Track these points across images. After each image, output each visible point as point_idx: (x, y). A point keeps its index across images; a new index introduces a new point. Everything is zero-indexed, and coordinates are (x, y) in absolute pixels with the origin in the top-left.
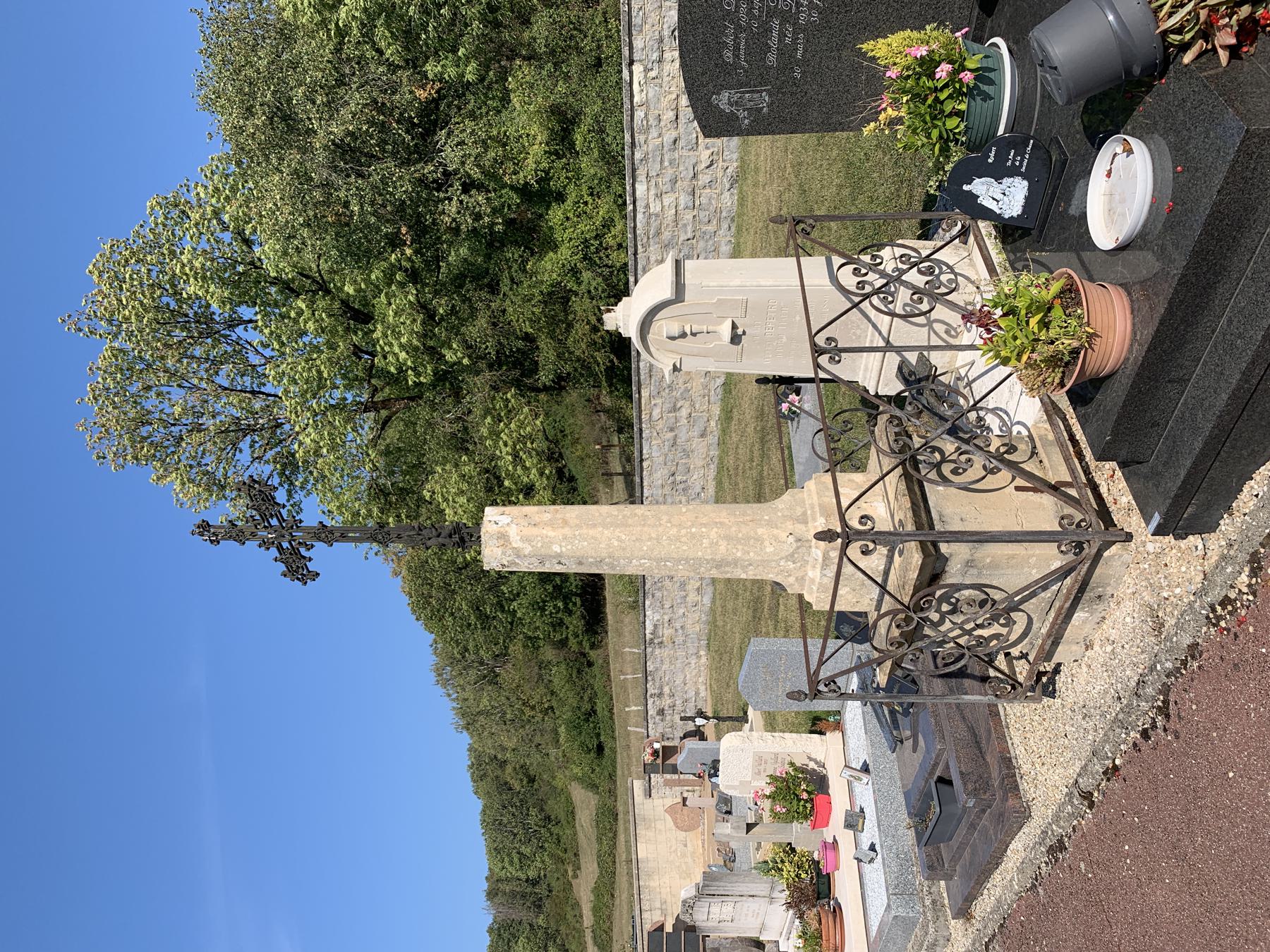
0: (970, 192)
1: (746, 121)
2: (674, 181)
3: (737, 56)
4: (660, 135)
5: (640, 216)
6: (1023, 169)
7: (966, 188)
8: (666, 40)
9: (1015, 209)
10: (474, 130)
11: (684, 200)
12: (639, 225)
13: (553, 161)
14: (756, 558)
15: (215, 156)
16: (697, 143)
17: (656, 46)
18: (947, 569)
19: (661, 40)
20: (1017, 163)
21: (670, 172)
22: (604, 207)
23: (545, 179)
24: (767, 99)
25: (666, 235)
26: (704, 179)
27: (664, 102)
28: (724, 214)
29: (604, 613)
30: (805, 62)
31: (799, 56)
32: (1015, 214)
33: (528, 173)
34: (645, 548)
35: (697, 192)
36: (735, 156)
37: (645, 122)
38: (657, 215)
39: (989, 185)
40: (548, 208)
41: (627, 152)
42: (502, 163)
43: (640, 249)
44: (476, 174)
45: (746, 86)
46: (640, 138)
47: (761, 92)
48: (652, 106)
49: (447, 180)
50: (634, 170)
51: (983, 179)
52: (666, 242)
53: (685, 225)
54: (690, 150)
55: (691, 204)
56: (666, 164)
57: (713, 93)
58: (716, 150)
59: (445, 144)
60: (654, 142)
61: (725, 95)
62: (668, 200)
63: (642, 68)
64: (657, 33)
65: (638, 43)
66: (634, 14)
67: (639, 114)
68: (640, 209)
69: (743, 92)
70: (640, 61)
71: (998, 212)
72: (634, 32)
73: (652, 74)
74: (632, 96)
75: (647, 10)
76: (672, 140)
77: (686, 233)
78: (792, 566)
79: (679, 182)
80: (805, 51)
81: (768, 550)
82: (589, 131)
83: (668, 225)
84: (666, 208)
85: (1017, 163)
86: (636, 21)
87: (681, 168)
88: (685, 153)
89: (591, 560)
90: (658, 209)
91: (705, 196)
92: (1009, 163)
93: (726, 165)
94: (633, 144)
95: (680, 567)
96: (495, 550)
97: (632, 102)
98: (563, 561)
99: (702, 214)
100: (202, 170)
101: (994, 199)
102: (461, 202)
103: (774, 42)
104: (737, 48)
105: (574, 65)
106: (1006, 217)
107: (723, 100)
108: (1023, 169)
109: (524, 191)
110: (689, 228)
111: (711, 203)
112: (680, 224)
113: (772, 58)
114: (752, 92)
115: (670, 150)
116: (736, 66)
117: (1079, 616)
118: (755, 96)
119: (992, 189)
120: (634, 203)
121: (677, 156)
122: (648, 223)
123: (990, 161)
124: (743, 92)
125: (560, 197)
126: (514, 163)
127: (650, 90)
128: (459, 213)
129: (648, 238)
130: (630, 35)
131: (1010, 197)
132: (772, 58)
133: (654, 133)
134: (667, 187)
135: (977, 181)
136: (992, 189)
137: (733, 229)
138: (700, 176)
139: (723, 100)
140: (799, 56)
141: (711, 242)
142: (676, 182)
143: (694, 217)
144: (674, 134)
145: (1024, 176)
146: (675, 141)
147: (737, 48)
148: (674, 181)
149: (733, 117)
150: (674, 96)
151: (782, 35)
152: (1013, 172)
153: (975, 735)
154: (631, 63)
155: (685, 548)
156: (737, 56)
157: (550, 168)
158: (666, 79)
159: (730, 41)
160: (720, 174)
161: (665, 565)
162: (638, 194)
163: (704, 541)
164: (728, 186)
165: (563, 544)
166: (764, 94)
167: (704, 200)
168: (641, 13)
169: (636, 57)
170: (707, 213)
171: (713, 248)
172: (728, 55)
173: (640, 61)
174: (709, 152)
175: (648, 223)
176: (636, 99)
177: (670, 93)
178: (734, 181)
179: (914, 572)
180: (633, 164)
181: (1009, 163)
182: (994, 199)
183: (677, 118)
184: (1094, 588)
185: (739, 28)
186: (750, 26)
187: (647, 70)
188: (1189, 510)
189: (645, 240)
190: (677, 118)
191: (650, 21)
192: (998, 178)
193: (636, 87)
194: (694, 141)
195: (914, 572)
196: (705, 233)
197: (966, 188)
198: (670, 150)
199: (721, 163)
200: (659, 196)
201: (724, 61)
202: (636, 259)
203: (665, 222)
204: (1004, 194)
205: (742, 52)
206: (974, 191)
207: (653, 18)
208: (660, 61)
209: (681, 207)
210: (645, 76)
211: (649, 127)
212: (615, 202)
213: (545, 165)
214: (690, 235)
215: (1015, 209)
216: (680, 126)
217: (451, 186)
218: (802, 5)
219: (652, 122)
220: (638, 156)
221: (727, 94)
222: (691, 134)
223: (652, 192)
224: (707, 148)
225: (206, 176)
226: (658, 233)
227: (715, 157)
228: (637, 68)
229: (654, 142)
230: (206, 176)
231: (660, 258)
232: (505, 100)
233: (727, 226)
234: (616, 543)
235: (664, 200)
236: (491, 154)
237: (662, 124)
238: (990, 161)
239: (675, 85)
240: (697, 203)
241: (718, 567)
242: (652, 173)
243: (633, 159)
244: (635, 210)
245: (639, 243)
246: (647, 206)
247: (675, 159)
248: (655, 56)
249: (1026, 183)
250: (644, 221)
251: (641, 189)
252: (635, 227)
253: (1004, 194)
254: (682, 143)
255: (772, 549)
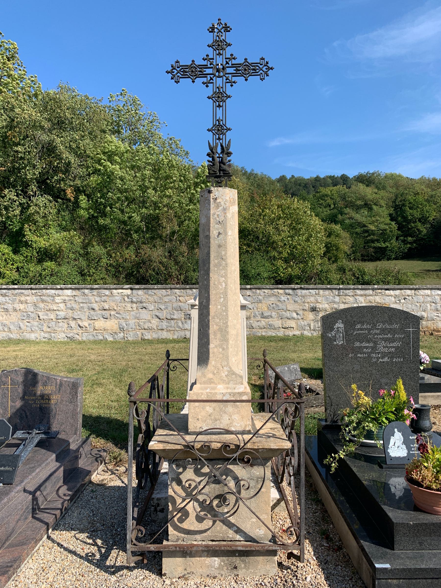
0: (394, 432)
1: (330, 335)
2: (72, 309)
3: (358, 330)
4: (96, 302)
5: (53, 291)
6: (411, 452)
7: (396, 430)
8: (141, 305)
9: (393, 454)
10: (51, 213)
11: (62, 314)
12: (48, 291)
13: (36, 250)
14: (230, 352)
15: (41, 86)
16: (92, 320)
17: (139, 300)
18: (255, 467)
19: (141, 302)
20: (413, 449)
21: (76, 306)
22: (15, 275)
23: (27, 245)
24: (340, 343)
25: (42, 305)
26: (73, 324)
27: (113, 304)
28: (53, 335)
29: (419, 260)
30: (356, 358)
31: (359, 355)
32: (391, 454)
33: (30, 236)
34: (231, 286)
35: (66, 321)
36: (84, 338)
37: (103, 295)
38: (53, 300)
39: (400, 440)
40: (8, 245)
41: (89, 286)
42: (35, 224)
43: (34, 291)
44: (32, 210)
45: (346, 334)
46: (95, 292)
47: (343, 341)
48: (110, 298)
49: (27, 196)
50: (78, 289)
51: (402, 436)
52: (38, 305)
53: (47, 315)
54: (88, 316)
55: (59, 317)
56: (81, 305)
57: (342, 321)
58: (88, 329)
59: (46, 198)
60: (92, 299)
61: (342, 325)
62: (62, 306)
63: (129, 294)
64: (144, 300)
65: (140, 292)
66: (153, 291)
67: (107, 292)
68: (57, 292)
69: (343, 333)
70: (132, 293)
71: (390, 446)
72: (145, 291)
73: (126, 299)
74: (116, 289)
75: (154, 296)
76: (94, 308)
77: (43, 315)
78: (223, 375)
79: (71, 311)
80: (360, 358)
81: (233, 359)
82: (53, 269)
83: (48, 306)
84: (58, 305)
85: (413, 449)
86: (150, 292)
87: (79, 312)
88: (87, 314)
89: (223, 253)
90: (57, 301)
91: (63, 325)
92: (412, 446)
93: (80, 334)
94: (92, 289)
95: (219, 307)
96: (228, 196)
97: (113, 289)
98: (221, 236)
99: (53, 323)
100: (36, 77)
101: (395, 443)
102: (15, 201)
103: (364, 344)
104: (361, 330)
105: (83, 263)
106: (388, 451)
107: (340, 325)
108: (411, 452)
109: (20, 233)
110: (45, 317)
111: (59, 327)
112: (49, 313)
113: (357, 344)
114: (343, 337)
115: (89, 307)
116: (354, 329)
117: (216, 561)
118: (341, 338)
119: (399, 441)
120: (61, 289)
121: (85, 310)
122: (49, 296)
123: (410, 437)
124: (343, 333)
125: (15, 252)
126: (35, 230)
127: (118, 298)
128: (10, 199)
129: (40, 296)
130: (144, 289)
131: (398, 450)
132: (357, 344)
133: (98, 299)
134: (69, 305)
135: (400, 434)
136: (399, 441)
137: (44, 340)
138: (74, 322)
139: (340, 325)
140: (359, 355)
141: (37, 328)
142: (71, 310)
143: (52, 319)
144: (97, 309)
145: (408, 453)
146: (93, 309)
147: (361, 330)
148: (72, 309)
149: (332, 329)
150: (115, 308)
151: (367, 348)
152: (409, 449)
153: (11, 533)
154: (132, 289)
155: (232, 309)
156: (358, 330)
157: (33, 248)
158: (124, 305)
159: (365, 326)
160: (75, 331)
161: (221, 298)
162: (66, 291)
163: (236, 321)
164: (68, 336)
165: (232, 237)
166: (342, 342)
167: (61, 324)
168: (153, 294)
169: (134, 291)
170: (54, 326)
171: (33, 330)
172: (359, 326)
173: (132, 293)
174: (87, 325)
175: (49, 296)
176: (114, 291)
177: (117, 306)
178: (72, 339)
179: (277, 446)
180: (82, 289)
181: (412, 446)
182: (395, 443)
183: (105, 310)
184: (242, 561)
185: (369, 330)
186: (371, 334)
187: (128, 296)
188: (395, 581)
189: (39, 294)
190: (105, 310)
191: (150, 297)
192: (404, 443)
193: (121, 291)
194: (93, 318)
195: (277, 446)
196: (42, 325)
197: (396, 430)
198: (89, 307)
199: (81, 332)
200: (64, 302)
201: (356, 324)
202: (28, 289)
203: (49, 305)
204: (398, 447)
205: (360, 332)
206: (395, 434)
207: (151, 299)
208: (132, 302)
209: (57, 312)
210: (125, 295)
211: (100, 297)
212: (16, 280)
213: (34, 245)
214: (41, 317)
215: (393, 454)
216: (101, 311)
217: (24, 198)
218: (378, 354)
219: (103, 298)
220: (86, 291)
221: (342, 326)
222: (97, 317)
223: (67, 298)
224: (89, 325)
225: (32, 77)
226: (43, 301)
227: (84, 329)
228: (129, 292)
229: (92, 299)
230: (32, 77)
231: (28, 302)
232: (65, 229)
233: (46, 336)
234: (233, 268)
235: (62, 304)
236: (40, 220)
237: (102, 303)
238: (410, 437)
239: (120, 309)
240: (60, 321)
241: (220, 330)
242: (77, 298)
243: (85, 289)
244: (57, 289)
245: (38, 291)
246: (59, 295)
247: (84, 309)
248: (134, 300)
249: (406, 455)
250: (51, 294)
251: (69, 292)
252: (47, 289)
253: (398, 447)
254: (92, 312)
255: (234, 361)
